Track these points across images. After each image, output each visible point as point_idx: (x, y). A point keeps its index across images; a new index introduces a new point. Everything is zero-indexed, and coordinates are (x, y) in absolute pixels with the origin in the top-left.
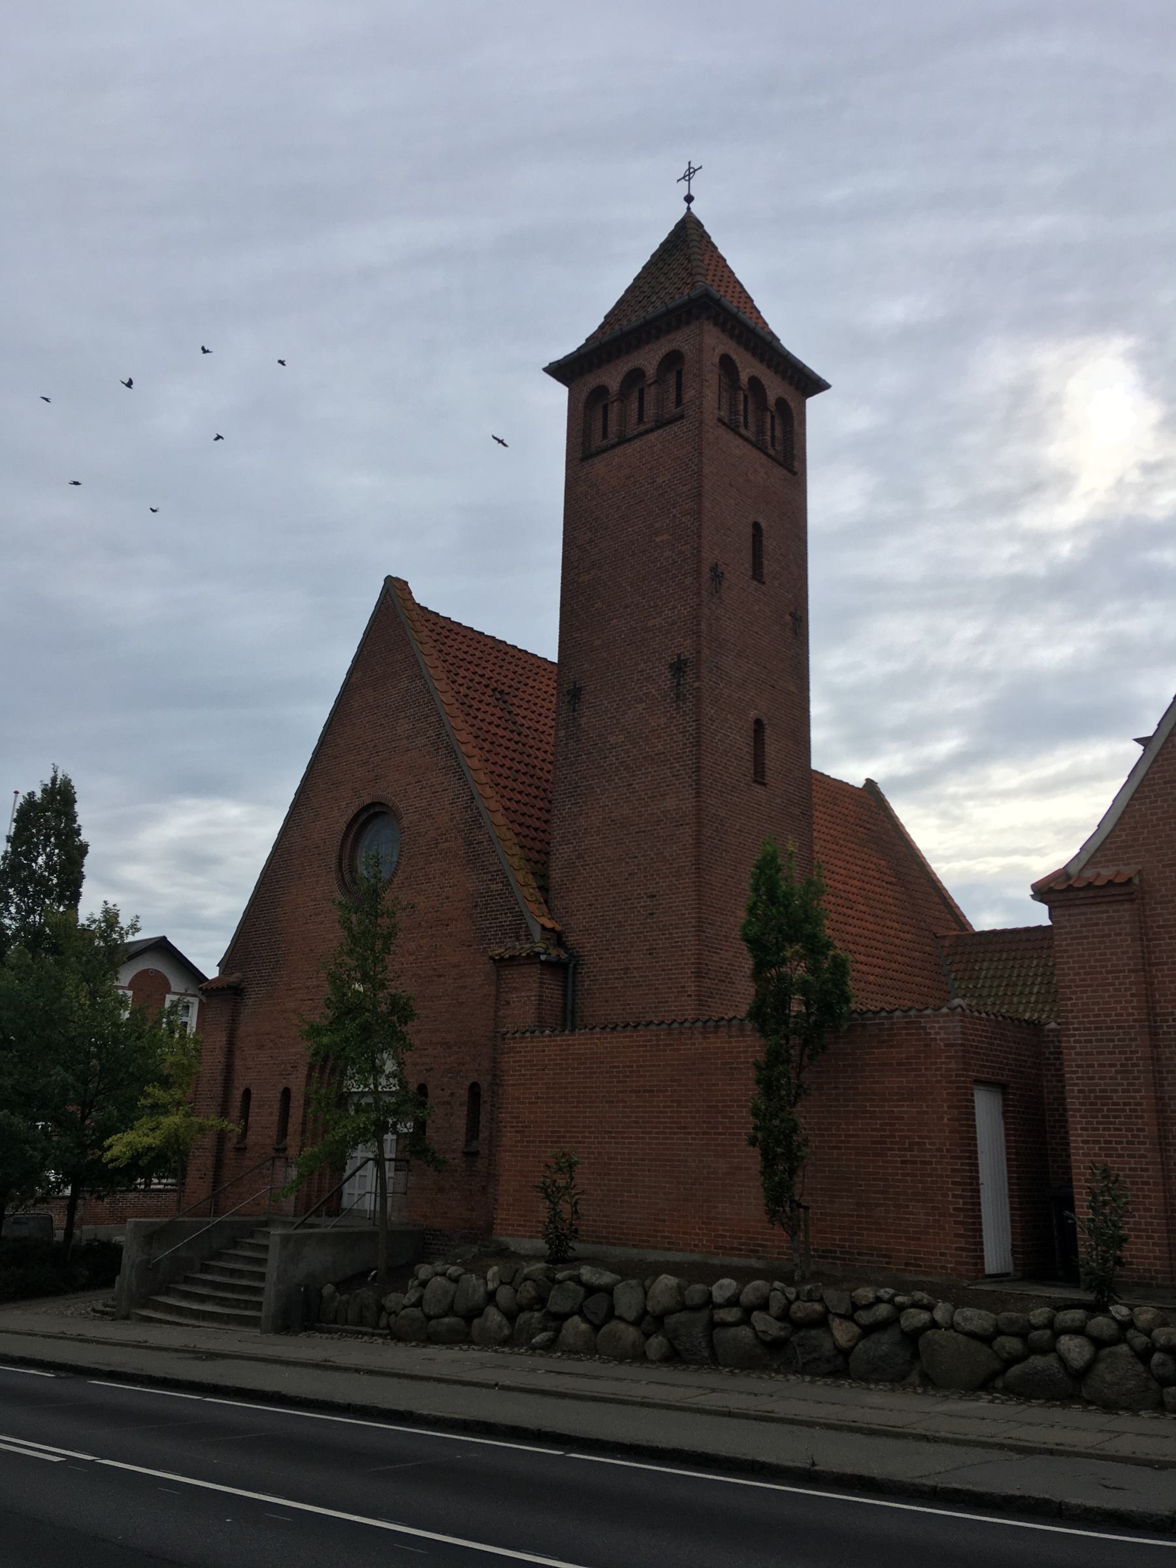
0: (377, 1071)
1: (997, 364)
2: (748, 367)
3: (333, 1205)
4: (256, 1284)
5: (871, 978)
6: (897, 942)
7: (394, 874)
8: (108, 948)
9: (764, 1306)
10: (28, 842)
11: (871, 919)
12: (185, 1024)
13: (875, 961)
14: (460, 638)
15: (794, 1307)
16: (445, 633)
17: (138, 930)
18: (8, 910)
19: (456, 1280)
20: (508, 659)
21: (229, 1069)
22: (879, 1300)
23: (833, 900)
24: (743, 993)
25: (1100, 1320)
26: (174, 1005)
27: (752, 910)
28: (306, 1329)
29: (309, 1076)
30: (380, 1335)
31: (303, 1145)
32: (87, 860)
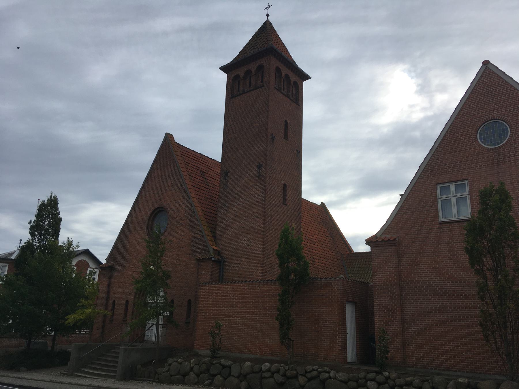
0: (158, 295)
1: (364, 71)
2: (285, 71)
3: (142, 338)
4: (115, 365)
5: (320, 267)
6: (329, 255)
7: (165, 231)
8: (69, 252)
9: (278, 372)
10: (42, 216)
11: (321, 248)
12: (94, 279)
13: (322, 262)
14: (190, 154)
15: (287, 372)
16: (185, 152)
17: (79, 247)
18: (35, 239)
19: (181, 363)
20: (206, 161)
21: (108, 293)
22: (314, 370)
23: (309, 241)
24: (277, 271)
25: (380, 376)
26: (91, 273)
27: (280, 245)
28: (131, 379)
29: (135, 297)
30: (155, 382)
31: (132, 319)
32: (62, 223)
